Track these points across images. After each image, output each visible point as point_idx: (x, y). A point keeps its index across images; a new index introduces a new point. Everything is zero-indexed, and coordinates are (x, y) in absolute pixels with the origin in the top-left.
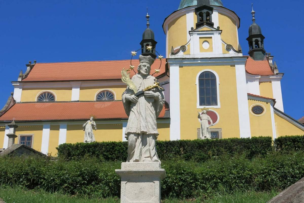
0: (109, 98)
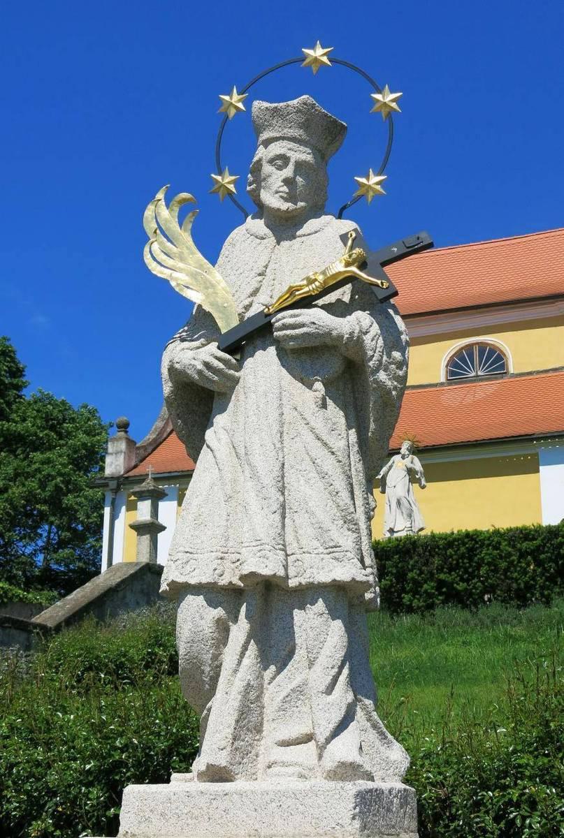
0: (487, 368)
